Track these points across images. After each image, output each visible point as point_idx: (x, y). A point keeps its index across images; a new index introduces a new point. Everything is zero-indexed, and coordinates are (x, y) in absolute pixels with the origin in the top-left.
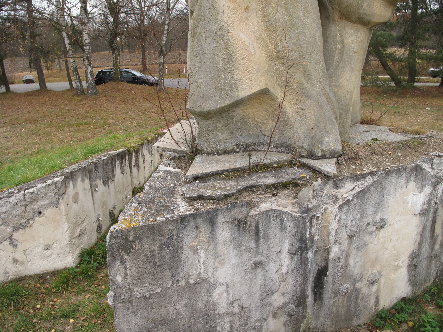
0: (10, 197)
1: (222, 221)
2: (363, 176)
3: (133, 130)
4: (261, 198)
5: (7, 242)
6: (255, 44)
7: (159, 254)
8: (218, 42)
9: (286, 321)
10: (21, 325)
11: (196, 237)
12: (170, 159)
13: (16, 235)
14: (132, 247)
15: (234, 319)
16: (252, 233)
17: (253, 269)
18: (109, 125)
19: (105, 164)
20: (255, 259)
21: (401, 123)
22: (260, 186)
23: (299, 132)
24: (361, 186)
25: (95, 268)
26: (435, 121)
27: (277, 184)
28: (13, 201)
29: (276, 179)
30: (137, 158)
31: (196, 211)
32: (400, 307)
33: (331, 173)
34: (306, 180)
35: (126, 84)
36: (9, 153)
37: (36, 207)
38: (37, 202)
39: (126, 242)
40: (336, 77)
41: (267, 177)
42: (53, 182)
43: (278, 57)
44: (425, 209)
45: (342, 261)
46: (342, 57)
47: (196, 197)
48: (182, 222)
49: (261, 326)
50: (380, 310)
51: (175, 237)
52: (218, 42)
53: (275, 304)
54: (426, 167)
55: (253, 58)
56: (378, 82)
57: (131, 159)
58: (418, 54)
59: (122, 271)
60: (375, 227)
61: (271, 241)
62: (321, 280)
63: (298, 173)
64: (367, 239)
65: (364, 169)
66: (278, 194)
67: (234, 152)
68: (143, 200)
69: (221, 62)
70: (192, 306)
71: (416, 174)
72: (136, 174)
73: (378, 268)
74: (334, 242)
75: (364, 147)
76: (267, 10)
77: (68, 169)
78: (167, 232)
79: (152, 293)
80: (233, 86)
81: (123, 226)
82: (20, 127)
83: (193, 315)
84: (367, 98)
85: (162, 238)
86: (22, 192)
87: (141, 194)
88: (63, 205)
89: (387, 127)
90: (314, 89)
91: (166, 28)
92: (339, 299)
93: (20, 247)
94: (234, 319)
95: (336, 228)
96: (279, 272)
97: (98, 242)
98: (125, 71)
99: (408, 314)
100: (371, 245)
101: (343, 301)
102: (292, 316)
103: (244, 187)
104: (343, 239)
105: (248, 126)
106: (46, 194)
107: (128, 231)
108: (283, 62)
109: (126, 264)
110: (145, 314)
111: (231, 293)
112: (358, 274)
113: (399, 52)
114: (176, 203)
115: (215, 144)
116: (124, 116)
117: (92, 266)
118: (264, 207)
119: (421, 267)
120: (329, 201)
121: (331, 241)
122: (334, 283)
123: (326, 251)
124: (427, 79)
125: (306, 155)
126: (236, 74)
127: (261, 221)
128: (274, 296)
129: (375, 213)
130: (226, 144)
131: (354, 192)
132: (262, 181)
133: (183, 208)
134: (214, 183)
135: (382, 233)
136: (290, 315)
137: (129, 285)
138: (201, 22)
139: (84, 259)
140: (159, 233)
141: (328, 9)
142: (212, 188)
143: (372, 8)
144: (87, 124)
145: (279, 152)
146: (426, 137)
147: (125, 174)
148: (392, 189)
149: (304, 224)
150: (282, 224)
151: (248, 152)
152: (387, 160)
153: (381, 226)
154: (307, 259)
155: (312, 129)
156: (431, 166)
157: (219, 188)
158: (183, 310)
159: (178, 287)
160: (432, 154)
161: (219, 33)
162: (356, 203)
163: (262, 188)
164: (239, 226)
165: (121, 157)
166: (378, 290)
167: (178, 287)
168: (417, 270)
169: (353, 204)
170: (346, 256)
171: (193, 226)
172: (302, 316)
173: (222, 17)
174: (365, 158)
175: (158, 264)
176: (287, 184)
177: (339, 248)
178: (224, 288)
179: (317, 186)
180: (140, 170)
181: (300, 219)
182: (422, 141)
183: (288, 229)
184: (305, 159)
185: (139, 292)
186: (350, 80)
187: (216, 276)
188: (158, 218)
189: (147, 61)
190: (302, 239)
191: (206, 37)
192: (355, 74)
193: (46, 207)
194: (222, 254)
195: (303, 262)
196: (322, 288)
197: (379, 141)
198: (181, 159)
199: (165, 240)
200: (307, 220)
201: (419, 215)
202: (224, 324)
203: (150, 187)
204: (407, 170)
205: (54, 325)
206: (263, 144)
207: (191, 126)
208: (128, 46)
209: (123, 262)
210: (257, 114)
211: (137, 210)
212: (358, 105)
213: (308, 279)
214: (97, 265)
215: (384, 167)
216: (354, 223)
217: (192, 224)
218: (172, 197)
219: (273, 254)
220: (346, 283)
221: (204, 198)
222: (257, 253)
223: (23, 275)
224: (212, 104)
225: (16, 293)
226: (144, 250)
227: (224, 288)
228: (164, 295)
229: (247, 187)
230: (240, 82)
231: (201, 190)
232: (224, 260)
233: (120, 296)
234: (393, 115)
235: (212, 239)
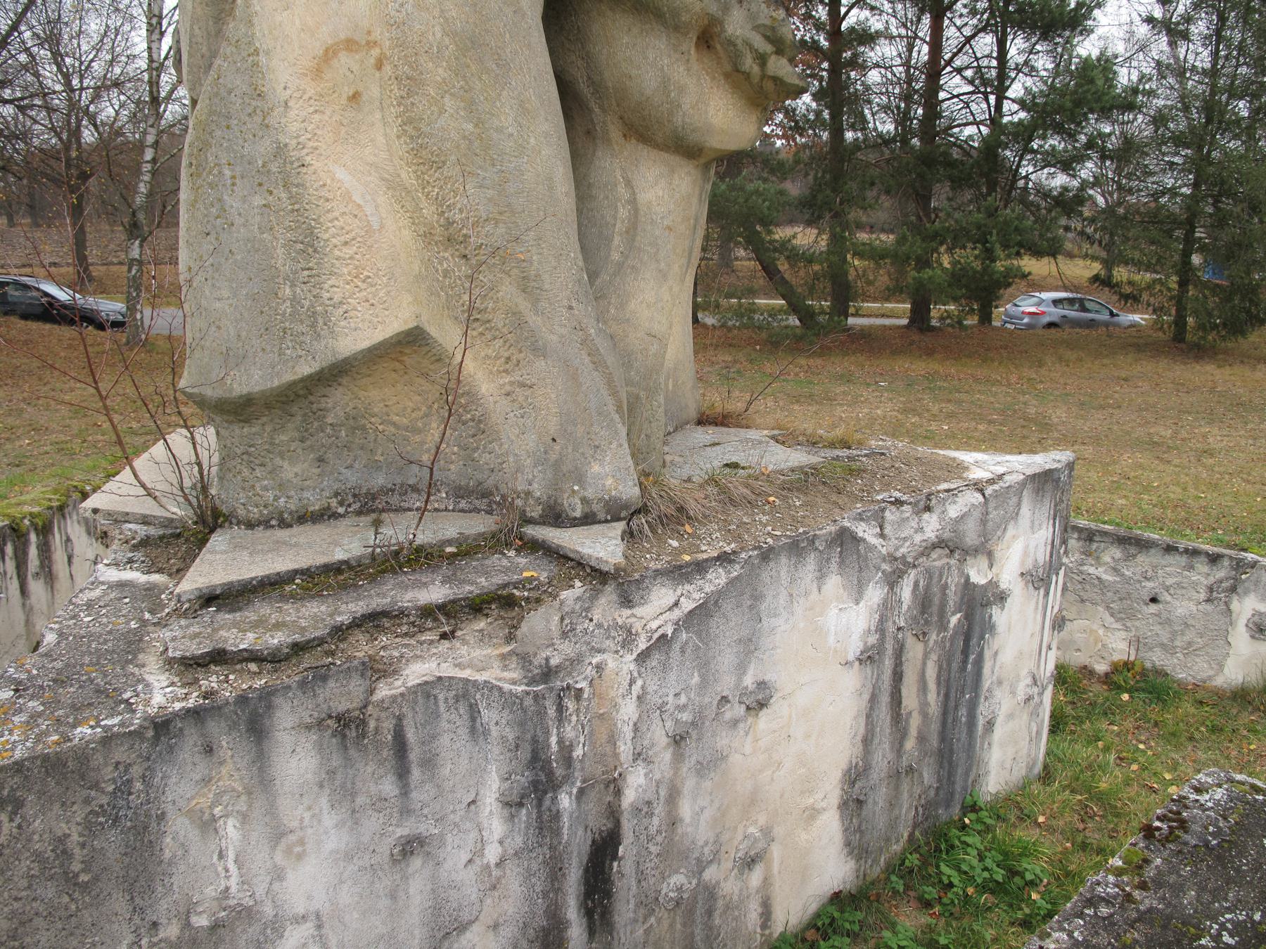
1: (289, 725)
2: (700, 568)
4: (406, 646)
6: (381, 200)
7: (83, 846)
8: (271, 193)
11: (206, 781)
12: (134, 546)
16: (385, 753)
17: (394, 861)
20: (400, 832)
21: (805, 419)
22: (402, 613)
23: (519, 451)
24: (696, 596)
26: (900, 417)
27: (453, 602)
29: (451, 588)
31: (205, 698)
32: (827, 921)
33: (607, 562)
34: (537, 588)
35: (21, 324)
40: (619, 296)
41: (425, 585)
43: (448, 237)
44: (873, 646)
45: (659, 809)
46: (633, 240)
47: (203, 656)
48: (157, 738)
50: (776, 935)
51: (138, 785)
52: (271, 193)
54: (866, 531)
55: (376, 242)
56: (756, 317)
57: (25, 553)
58: (853, 244)
60: (743, 707)
61: (446, 772)
62: (603, 872)
63: (516, 569)
64: (722, 741)
65: (704, 548)
66: (459, 633)
67: (330, 517)
68: (31, 678)
69: (280, 251)
71: (841, 552)
72: (44, 600)
73: (762, 820)
74: (631, 758)
75: (701, 486)
76: (413, 104)
78: (108, 772)
80: (321, 321)
84: (729, 358)
85: (93, 793)
89: (766, 432)
90: (554, 327)
91: (149, 155)
92: (659, 921)
95: (635, 717)
96: (478, 861)
98: (16, 283)
99: (848, 936)
100: (735, 758)
101: (671, 926)
103: (354, 618)
104: (656, 749)
108: (464, 252)
112: (706, 843)
113: (805, 237)
115: (270, 495)
116: (10, 421)
118: (417, 672)
119: (875, 803)
120: (608, 642)
121: (623, 758)
122: (641, 877)
123: (612, 786)
124: (879, 308)
125: (541, 516)
126: (326, 286)
127: (410, 715)
128: (468, 935)
129: (741, 668)
130: (306, 494)
131: (677, 614)
132: (409, 595)
133: (161, 692)
135: (764, 721)
138: (218, 133)
140: (83, 777)
141: (590, 111)
142: (255, 626)
143: (706, 112)
145: (462, 511)
146: (866, 455)
148: (783, 599)
149: (542, 713)
150: (473, 719)
151: (374, 516)
152: (764, 519)
153: (759, 702)
154: (557, 816)
155: (554, 440)
156: (878, 530)
157: (278, 626)
160: (879, 498)
161: (274, 168)
162: (686, 643)
163: (407, 616)
164: (344, 736)
166: (767, 882)
168: (864, 813)
169: (676, 647)
170: (670, 795)
171: (195, 745)
173: (283, 120)
174: (705, 517)
175: (84, 878)
176: (483, 602)
177: (646, 775)
178: (308, 929)
179: (570, 602)
180: (57, 586)
181: (529, 701)
182: (854, 465)
183: (494, 731)
184: (537, 528)
186: (660, 306)
188: (79, 729)
189: (93, 254)
190: (537, 759)
191: (233, 177)
192: (671, 289)
194: (295, 824)
195: (547, 824)
196: (608, 894)
197: (743, 468)
198: (168, 544)
199: (104, 800)
200: (547, 703)
201: (857, 663)
203: (61, 634)
204: (817, 544)
207: (194, 444)
208: (31, 207)
210: (395, 402)
212: (687, 374)
213: (564, 875)
215: (755, 538)
216: (683, 699)
217: (191, 740)
218: (131, 662)
219: (453, 812)
220: (677, 872)
221: (228, 656)
222: (406, 812)
224: (257, 374)
226: (29, 840)
227: (308, 929)
229: (363, 616)
230: (341, 311)
231: (223, 633)
232: (301, 842)
234: (798, 401)
235: (261, 782)
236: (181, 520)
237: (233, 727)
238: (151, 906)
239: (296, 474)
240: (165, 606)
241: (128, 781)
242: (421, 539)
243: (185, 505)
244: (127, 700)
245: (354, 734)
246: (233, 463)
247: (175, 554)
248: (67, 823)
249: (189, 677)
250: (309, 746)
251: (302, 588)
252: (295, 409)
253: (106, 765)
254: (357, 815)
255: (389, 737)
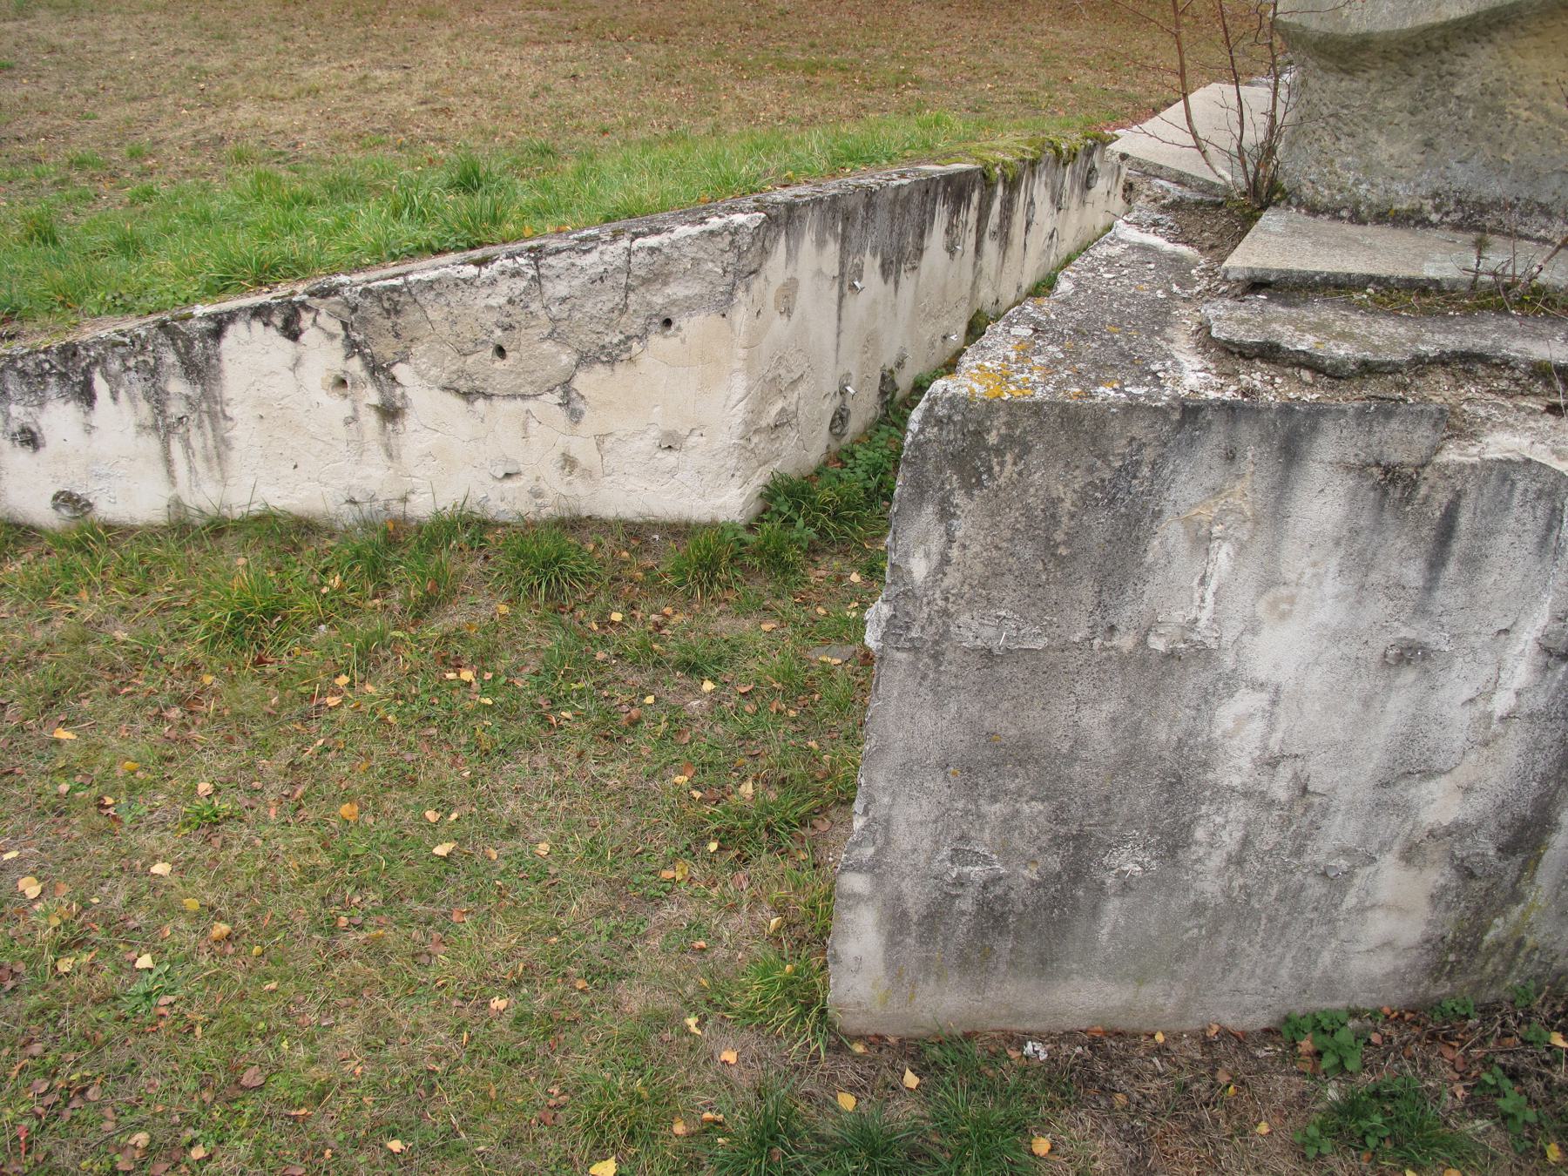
0: (585, 252)
1: (1328, 458)
3: (1000, 113)
5: (555, 398)
7: (1072, 516)
9: (1445, 889)
10: (562, 657)
11: (1216, 491)
12: (1163, 206)
13: (582, 381)
14: (990, 469)
15: (1264, 819)
16: (1425, 531)
17: (1385, 664)
18: (918, 82)
19: (901, 201)
20: (1405, 632)
22: (1506, 363)
25: (805, 546)
28: (591, 266)
30: (1008, 206)
31: (1244, 395)
36: (578, 128)
37: (659, 300)
38: (665, 284)
39: (973, 445)
42: (725, 227)
49: (1350, 873)
53: (1422, 816)
57: (989, 207)
59: (936, 545)
68: (1049, 322)
70: (1136, 730)
72: (994, 264)
77: (781, 196)
78: (1120, 446)
79: (1013, 646)
81: (977, 388)
82: (620, 50)
83: (1127, 762)
85: (1099, 463)
86: (624, 243)
87: (1047, 303)
88: (743, 309)
93: (590, 424)
94: (1264, 819)
96: (1481, 705)
97: (826, 463)
102: (1472, 875)
105: (1507, 127)
106: (696, 262)
107: (990, 407)
109: (955, 523)
110: (974, 709)
111: (1282, 725)
114: (1168, 356)
115: (1350, 177)
116: (973, 59)
117: (796, 535)
118: (1501, 444)
127: (1473, 496)
130: (1397, 186)
132: (1518, 344)
133: (1193, 375)
134: (1324, 315)
136: (1467, 873)
137: (946, 599)
139: (774, 508)
140: (1094, 441)
142: (1316, 328)
144: (842, 70)
147: (958, 255)
150: (1549, 528)
157: (1344, 336)
158: (1100, 734)
159: (1106, 649)
163: (1513, 369)
164: (1385, 493)
165: (956, 189)
167: (1106, 649)
171: (1218, 446)
172: (1510, 890)
175: (1063, 551)
178: (1261, 699)
180: (1009, 253)
185: (971, 630)
187: (1247, 651)
188: (1101, 389)
193: (690, 305)
194: (1292, 576)
198: (1205, 212)
199: (1107, 475)
202: (1224, 827)
203: (1078, 284)
205: (654, 682)
206: (1546, 211)
209: (946, 514)
211: (1026, 351)
214: (815, 536)
217: (1216, 439)
218: (1157, 333)
219: (1478, 633)
222: (1421, 611)
223: (585, 514)
225: (557, 560)
226: (1025, 491)
227: (1261, 699)
228: (1053, 666)
229: (1454, 352)
231: (1276, 326)
232: (1291, 600)
233: (908, 628)
235: (1274, 514)
236: (1226, 188)
237: (1265, 438)
238: (1115, 607)
239: (1391, 156)
240: (1195, 283)
241: (1137, 461)
242: (1543, 278)
243: (1238, 169)
244: (1154, 373)
245: (1398, 496)
246: (1313, 126)
247: (1212, 227)
248: (1066, 486)
249: (1228, 368)
250: (1341, 491)
251: (1374, 300)
252: (1417, 66)
253: (1121, 436)
254: (1364, 593)
255: (1438, 514)
